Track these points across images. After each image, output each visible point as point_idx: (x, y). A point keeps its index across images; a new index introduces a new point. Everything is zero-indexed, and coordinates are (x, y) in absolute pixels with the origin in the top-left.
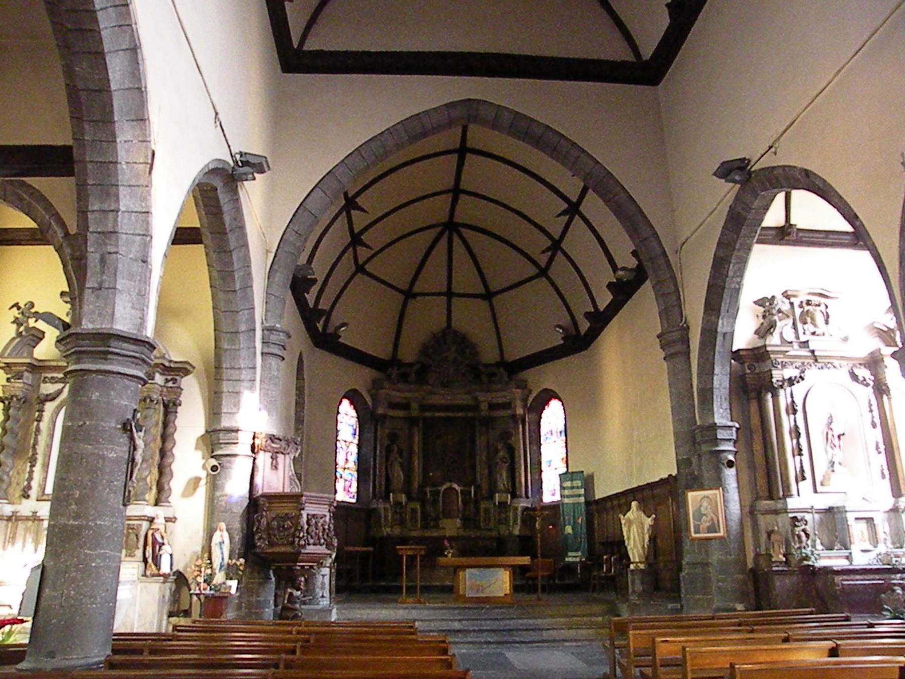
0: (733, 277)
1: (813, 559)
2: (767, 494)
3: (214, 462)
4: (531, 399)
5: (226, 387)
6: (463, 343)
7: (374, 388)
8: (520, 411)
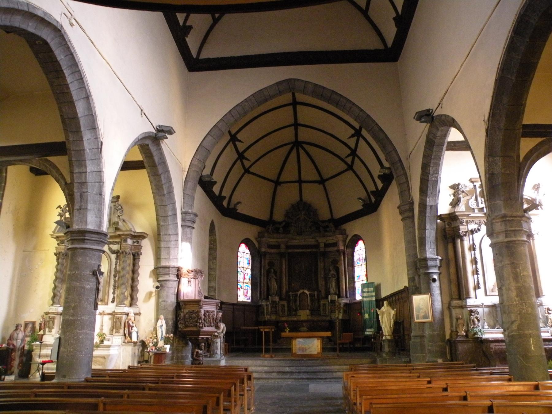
0: (433, 174)
1: (479, 333)
2: (457, 297)
3: (158, 284)
4: (348, 241)
5: (163, 244)
7: (259, 237)
8: (342, 248)
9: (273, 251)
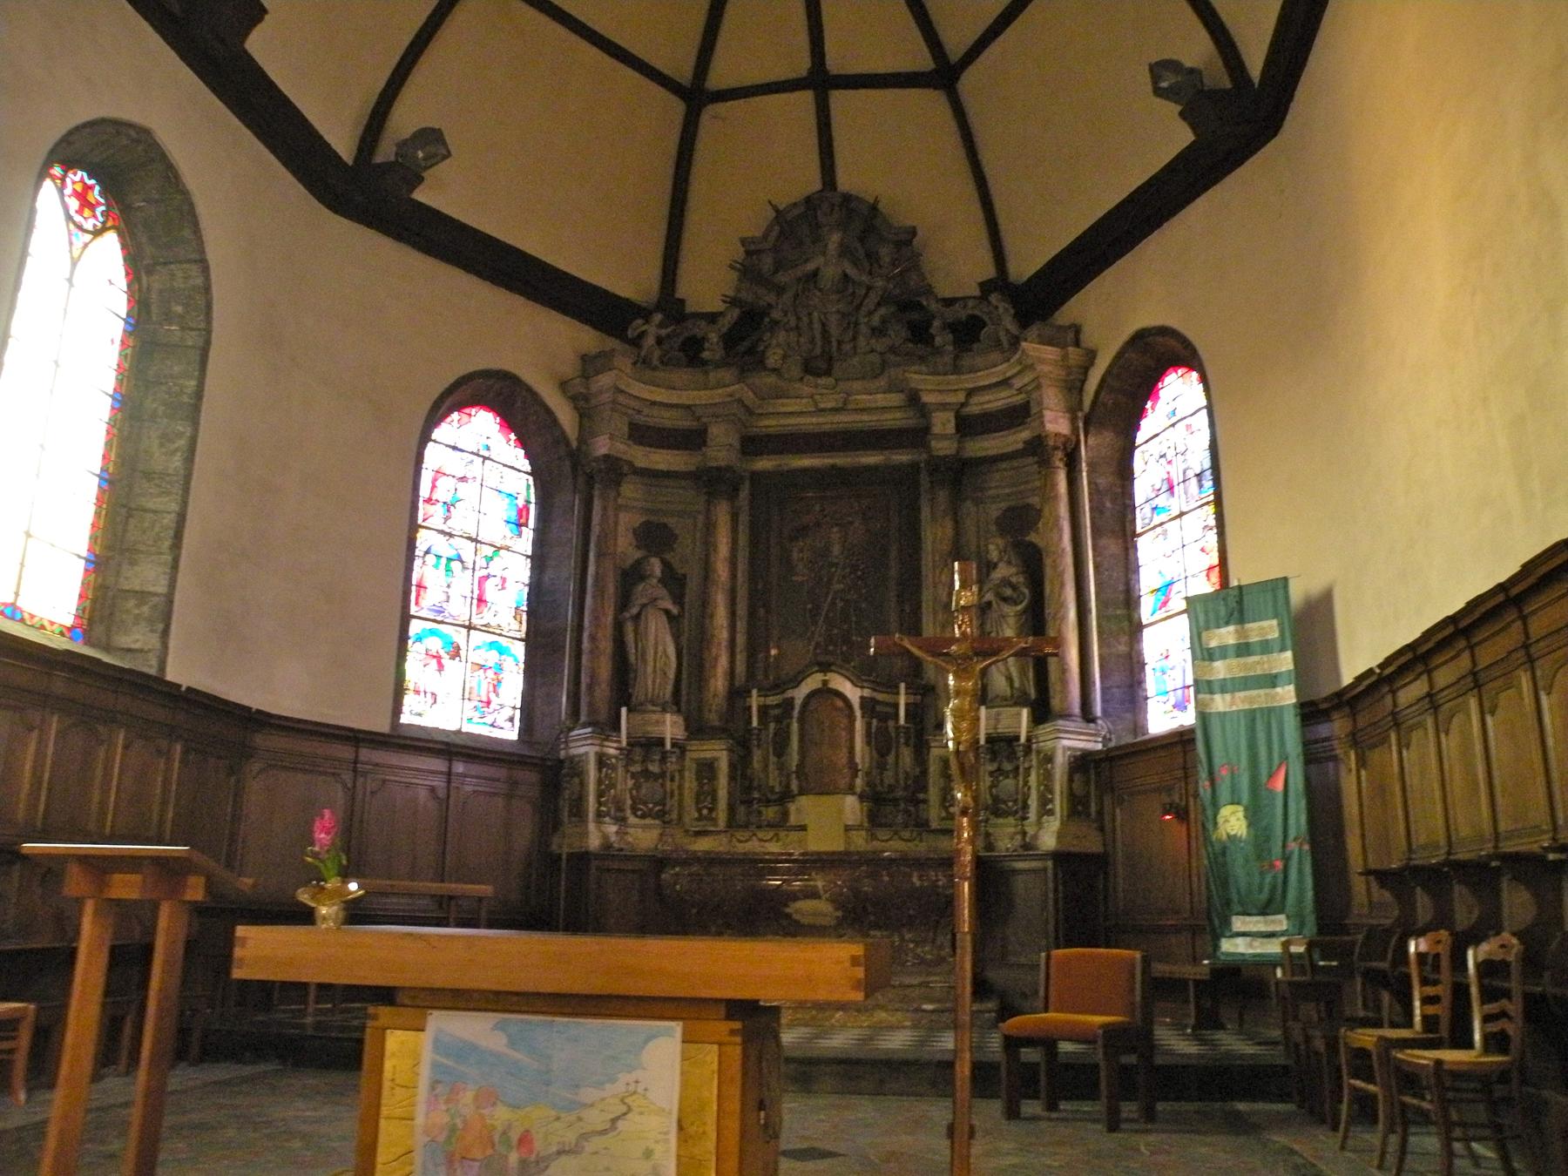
6: (865, 224)
8: (1056, 423)
9: (663, 460)
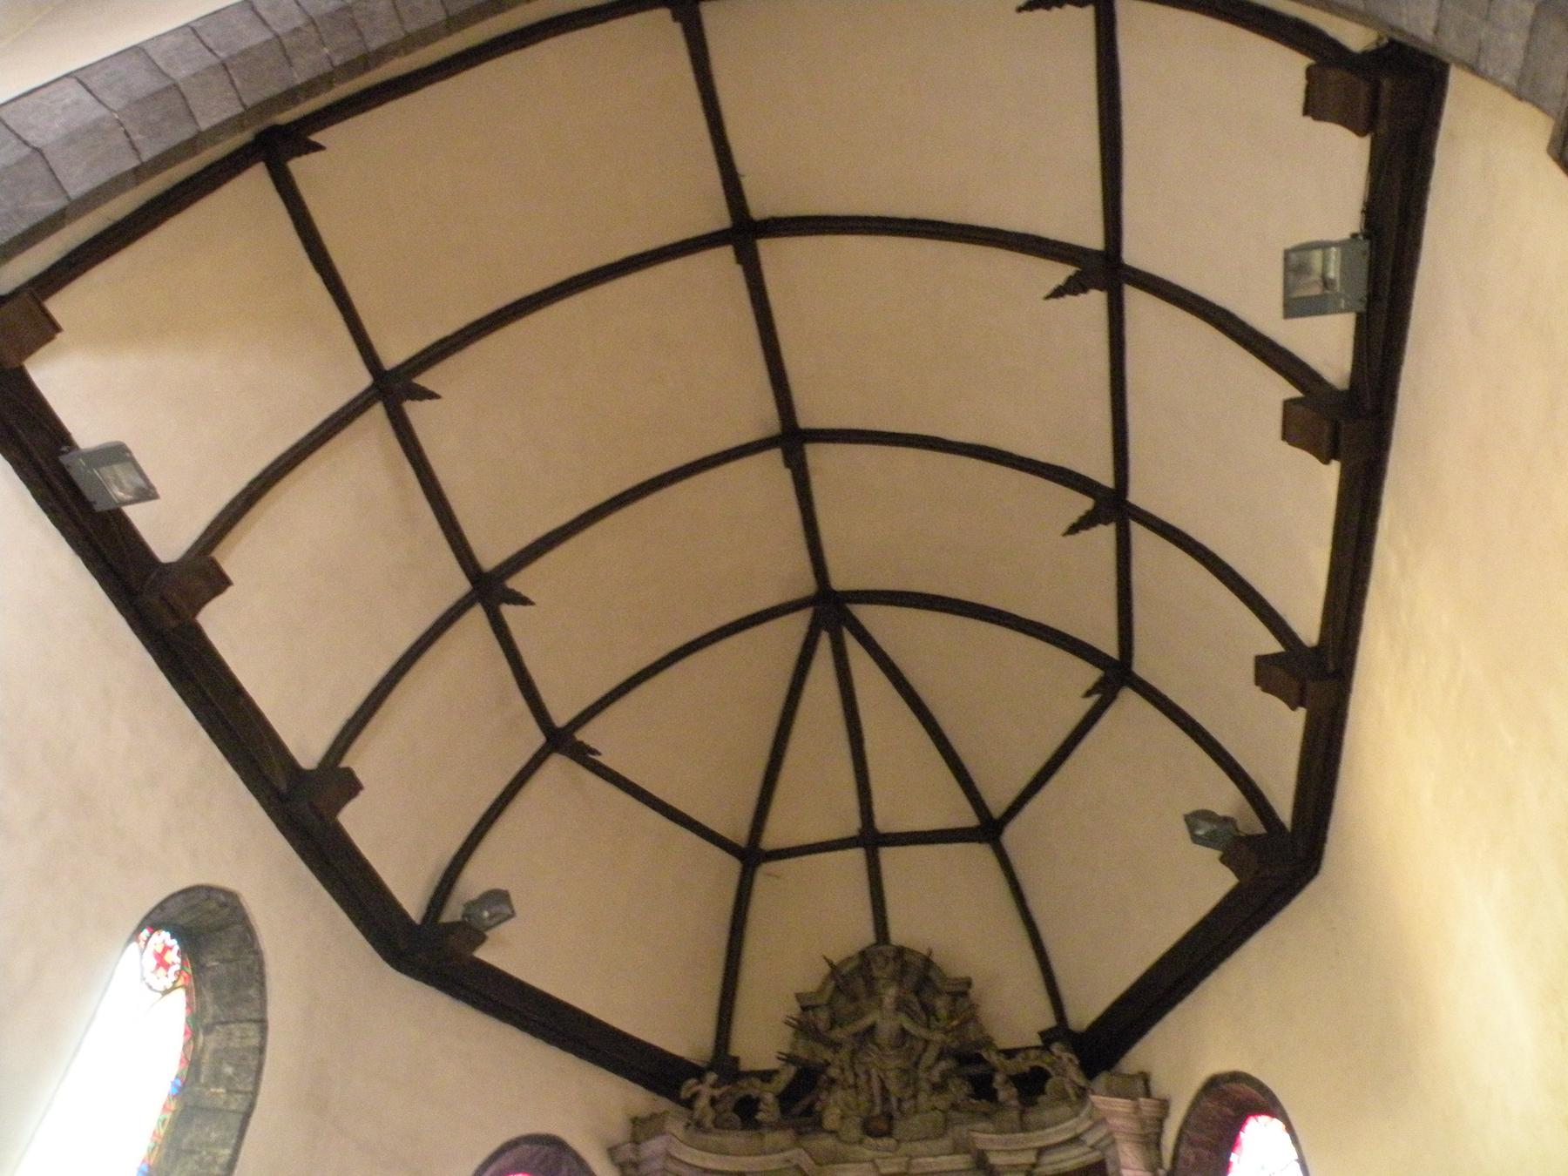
6: (921, 978)
